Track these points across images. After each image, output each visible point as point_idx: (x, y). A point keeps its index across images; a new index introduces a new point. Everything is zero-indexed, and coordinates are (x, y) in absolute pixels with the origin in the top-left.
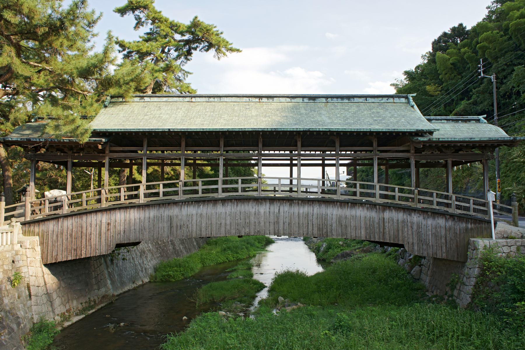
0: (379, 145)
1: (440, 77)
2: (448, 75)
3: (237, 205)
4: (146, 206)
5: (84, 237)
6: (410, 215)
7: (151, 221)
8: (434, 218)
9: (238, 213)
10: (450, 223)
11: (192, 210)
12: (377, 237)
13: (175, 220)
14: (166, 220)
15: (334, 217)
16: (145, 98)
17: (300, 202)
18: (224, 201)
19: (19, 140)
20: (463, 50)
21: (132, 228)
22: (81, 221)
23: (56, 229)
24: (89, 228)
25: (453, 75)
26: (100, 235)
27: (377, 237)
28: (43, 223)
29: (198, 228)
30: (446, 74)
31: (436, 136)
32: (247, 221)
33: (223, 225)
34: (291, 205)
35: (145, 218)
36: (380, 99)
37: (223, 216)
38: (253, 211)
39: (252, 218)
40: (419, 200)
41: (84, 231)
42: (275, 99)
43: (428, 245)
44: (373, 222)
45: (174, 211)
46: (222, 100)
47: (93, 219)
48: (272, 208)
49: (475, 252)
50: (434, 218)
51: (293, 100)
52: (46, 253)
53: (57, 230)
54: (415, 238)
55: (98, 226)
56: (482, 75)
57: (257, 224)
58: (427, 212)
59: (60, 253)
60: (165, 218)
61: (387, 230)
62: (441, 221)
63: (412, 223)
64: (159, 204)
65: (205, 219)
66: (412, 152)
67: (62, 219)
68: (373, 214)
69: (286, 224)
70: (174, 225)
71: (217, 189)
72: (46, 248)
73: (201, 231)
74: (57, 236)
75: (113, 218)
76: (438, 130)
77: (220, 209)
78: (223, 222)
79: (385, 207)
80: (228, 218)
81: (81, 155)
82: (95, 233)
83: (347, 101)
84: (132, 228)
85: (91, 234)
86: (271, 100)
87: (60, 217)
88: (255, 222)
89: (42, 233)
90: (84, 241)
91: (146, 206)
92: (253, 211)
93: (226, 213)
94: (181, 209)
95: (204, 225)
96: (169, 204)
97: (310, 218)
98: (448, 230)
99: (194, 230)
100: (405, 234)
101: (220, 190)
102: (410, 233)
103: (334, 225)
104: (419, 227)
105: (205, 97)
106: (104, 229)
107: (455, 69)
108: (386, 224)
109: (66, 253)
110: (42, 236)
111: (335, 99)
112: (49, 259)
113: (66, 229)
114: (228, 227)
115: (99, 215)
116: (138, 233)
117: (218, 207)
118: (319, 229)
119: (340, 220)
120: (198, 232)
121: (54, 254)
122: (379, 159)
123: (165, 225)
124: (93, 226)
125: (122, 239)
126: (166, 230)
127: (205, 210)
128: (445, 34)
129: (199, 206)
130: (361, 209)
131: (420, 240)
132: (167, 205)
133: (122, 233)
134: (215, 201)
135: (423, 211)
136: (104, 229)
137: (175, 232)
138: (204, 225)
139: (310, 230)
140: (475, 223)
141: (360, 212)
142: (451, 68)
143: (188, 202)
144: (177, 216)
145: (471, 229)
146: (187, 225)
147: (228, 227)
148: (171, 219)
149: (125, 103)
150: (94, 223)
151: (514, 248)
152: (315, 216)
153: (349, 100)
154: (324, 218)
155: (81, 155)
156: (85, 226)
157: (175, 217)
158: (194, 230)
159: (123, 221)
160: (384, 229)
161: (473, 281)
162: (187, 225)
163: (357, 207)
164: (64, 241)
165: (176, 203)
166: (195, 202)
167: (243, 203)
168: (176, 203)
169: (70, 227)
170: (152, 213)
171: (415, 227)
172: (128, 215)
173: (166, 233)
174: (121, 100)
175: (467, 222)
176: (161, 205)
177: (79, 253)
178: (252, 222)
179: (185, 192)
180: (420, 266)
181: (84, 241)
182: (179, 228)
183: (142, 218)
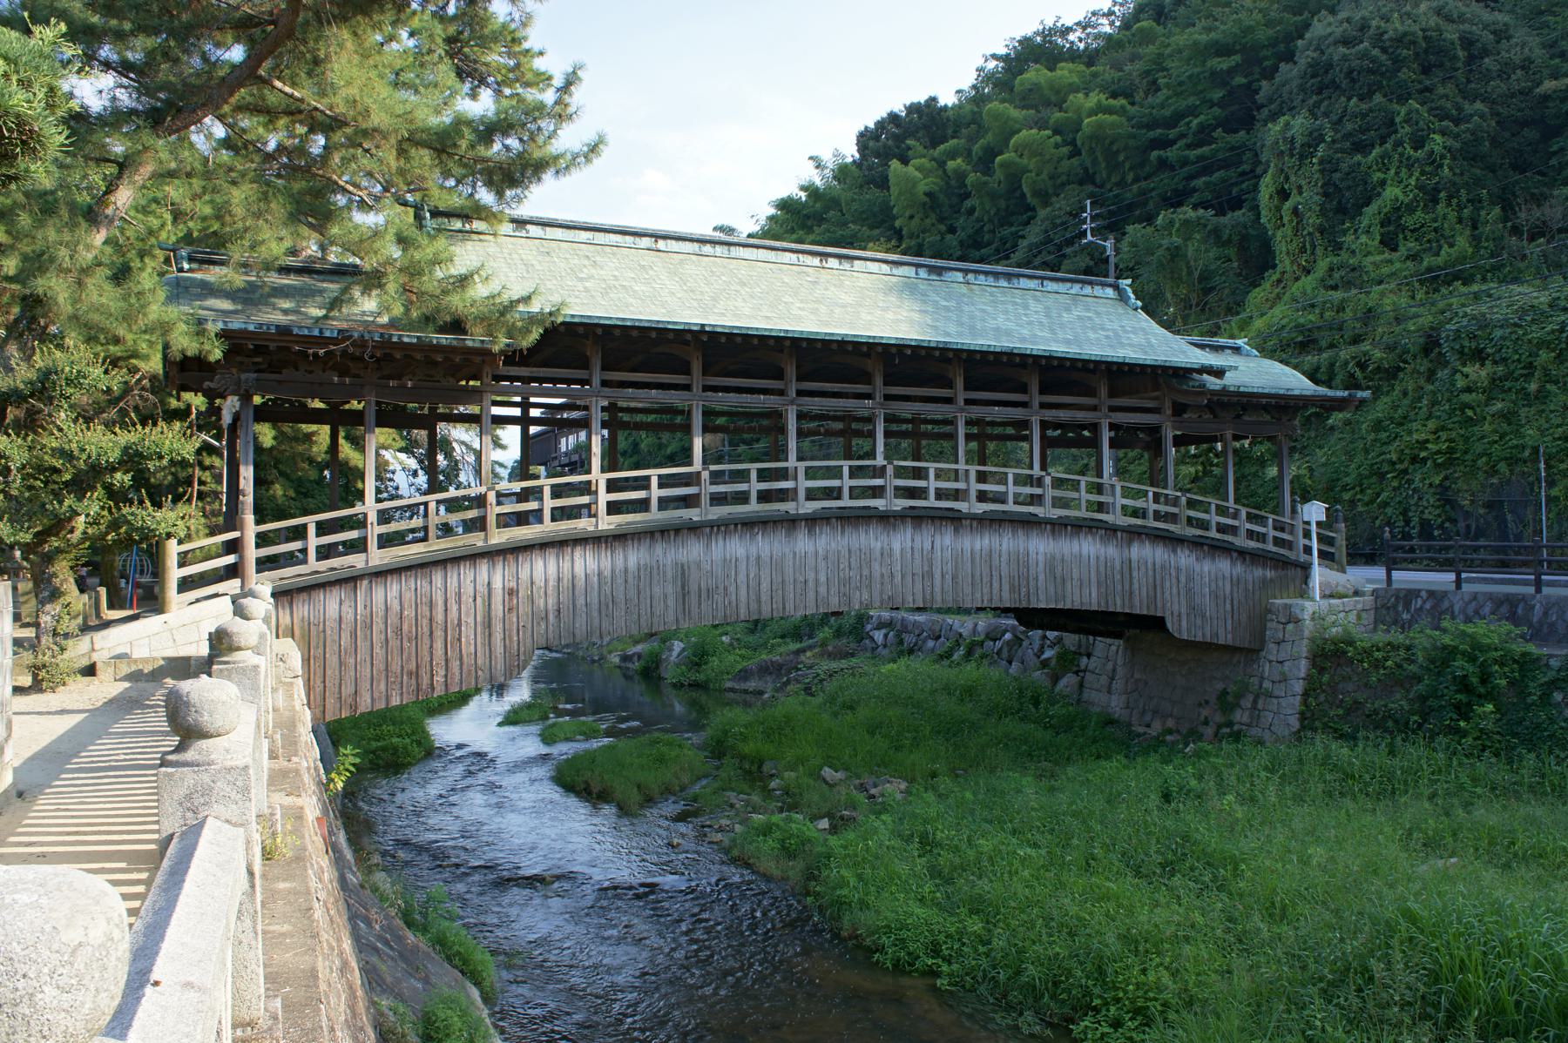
0: (1112, 394)
1: (897, 224)
2: (916, 220)
3: (843, 533)
4: (618, 538)
5: (439, 633)
6: (1174, 551)
7: (630, 580)
8: (1213, 559)
9: (845, 552)
10: (1239, 569)
11: (736, 547)
12: (1119, 602)
13: (694, 576)
14: (669, 575)
15: (1041, 558)
16: (529, 227)
17: (975, 524)
18: (812, 521)
19: (251, 328)
20: (951, 164)
21: (581, 601)
22: (426, 584)
23: (348, 615)
24: (454, 608)
25: (928, 221)
26: (488, 624)
27: (1119, 602)
28: (304, 595)
29: (753, 596)
30: (911, 217)
31: (1231, 380)
32: (866, 572)
33: (811, 584)
34: (956, 530)
35: (613, 571)
36: (1069, 285)
37: (811, 561)
38: (877, 546)
39: (876, 566)
40: (1189, 519)
41: (440, 617)
42: (857, 263)
43: (1203, 616)
44: (1113, 568)
45: (692, 551)
46: (733, 254)
47: (469, 579)
48: (918, 539)
49: (1290, 627)
50: (1213, 559)
51: (895, 271)
52: (319, 689)
53: (350, 616)
54: (1184, 602)
55: (479, 600)
56: (1089, 237)
57: (887, 580)
58: (1202, 545)
59: (365, 685)
60: (669, 569)
61: (1136, 586)
62: (1224, 565)
63: (1178, 569)
64: (652, 533)
65: (768, 571)
66: (1169, 412)
67: (365, 582)
68: (1111, 551)
69: (948, 577)
70: (693, 588)
71: (840, 489)
72: (320, 672)
73: (759, 602)
74: (354, 634)
75: (524, 574)
76: (1236, 368)
77: (803, 543)
78: (811, 576)
79: (1134, 534)
80: (822, 565)
81: (410, 384)
82: (471, 620)
83: (1005, 284)
84: (581, 601)
85: (459, 625)
86: (846, 265)
87: (361, 577)
88: (882, 575)
89: (302, 628)
90: (439, 645)
91: (618, 538)
92: (877, 546)
93: (816, 553)
94: (708, 545)
95: (765, 586)
96: (677, 531)
97: (996, 562)
98: (1236, 582)
99: (743, 598)
100: (1167, 594)
101: (705, 500)
102: (1175, 591)
103: (1042, 577)
104: (1190, 579)
105: (692, 240)
106: (498, 608)
107: (932, 208)
108: (1135, 574)
109: (383, 687)
110: (303, 636)
111: (982, 277)
112: (328, 706)
113: (381, 613)
114: (823, 590)
115: (483, 567)
116: (595, 614)
117: (800, 536)
118: (1012, 589)
119: (1051, 564)
120: (754, 606)
121: (348, 690)
122: (969, 423)
123: (670, 589)
124: (464, 598)
125: (551, 636)
126: (671, 602)
127: (765, 545)
128: (893, 117)
129: (753, 536)
130: (1090, 538)
131: (1192, 608)
132: (658, 535)
133: (551, 617)
134: (791, 523)
135: (1196, 544)
136: (498, 608)
137: (695, 610)
138: (765, 586)
139: (995, 591)
140: (1276, 568)
141: (1088, 547)
142: (924, 204)
143: (727, 525)
144: (699, 565)
145: (1271, 580)
146: (725, 589)
147: (823, 590)
148: (683, 572)
149: (475, 237)
150: (468, 589)
151: (1352, 617)
152: (1004, 558)
153: (1009, 281)
154: (1021, 561)
155: (410, 384)
156: (440, 602)
157: (693, 567)
158: (743, 598)
159: (552, 583)
160: (1131, 584)
161: (1299, 687)
162: (725, 589)
163: (1082, 536)
164: (377, 650)
165: (693, 528)
166: (745, 524)
167: (856, 527)
168: (693, 528)
169: (396, 606)
170: (633, 557)
171: (1183, 579)
172: (566, 565)
173: (671, 612)
174: (458, 225)
175: (1264, 566)
176: (658, 535)
177: (425, 681)
178: (877, 575)
179: (664, 503)
180: (1077, 673)
181: (439, 645)
182: (704, 596)
183: (607, 573)
